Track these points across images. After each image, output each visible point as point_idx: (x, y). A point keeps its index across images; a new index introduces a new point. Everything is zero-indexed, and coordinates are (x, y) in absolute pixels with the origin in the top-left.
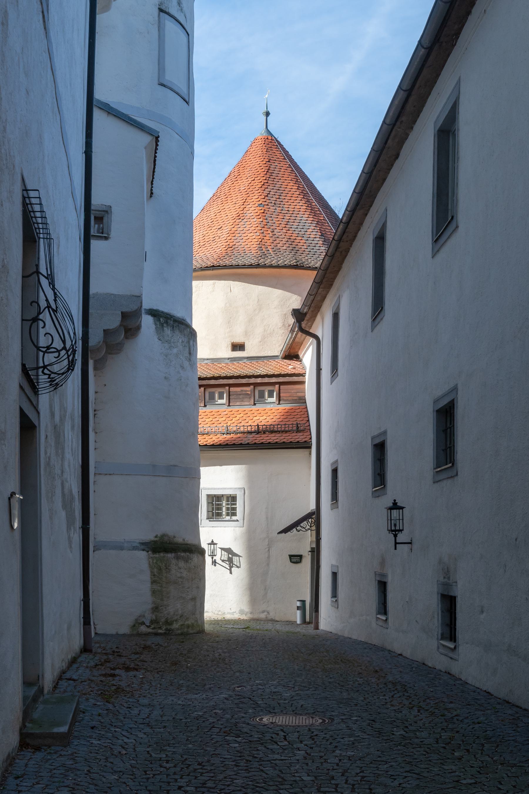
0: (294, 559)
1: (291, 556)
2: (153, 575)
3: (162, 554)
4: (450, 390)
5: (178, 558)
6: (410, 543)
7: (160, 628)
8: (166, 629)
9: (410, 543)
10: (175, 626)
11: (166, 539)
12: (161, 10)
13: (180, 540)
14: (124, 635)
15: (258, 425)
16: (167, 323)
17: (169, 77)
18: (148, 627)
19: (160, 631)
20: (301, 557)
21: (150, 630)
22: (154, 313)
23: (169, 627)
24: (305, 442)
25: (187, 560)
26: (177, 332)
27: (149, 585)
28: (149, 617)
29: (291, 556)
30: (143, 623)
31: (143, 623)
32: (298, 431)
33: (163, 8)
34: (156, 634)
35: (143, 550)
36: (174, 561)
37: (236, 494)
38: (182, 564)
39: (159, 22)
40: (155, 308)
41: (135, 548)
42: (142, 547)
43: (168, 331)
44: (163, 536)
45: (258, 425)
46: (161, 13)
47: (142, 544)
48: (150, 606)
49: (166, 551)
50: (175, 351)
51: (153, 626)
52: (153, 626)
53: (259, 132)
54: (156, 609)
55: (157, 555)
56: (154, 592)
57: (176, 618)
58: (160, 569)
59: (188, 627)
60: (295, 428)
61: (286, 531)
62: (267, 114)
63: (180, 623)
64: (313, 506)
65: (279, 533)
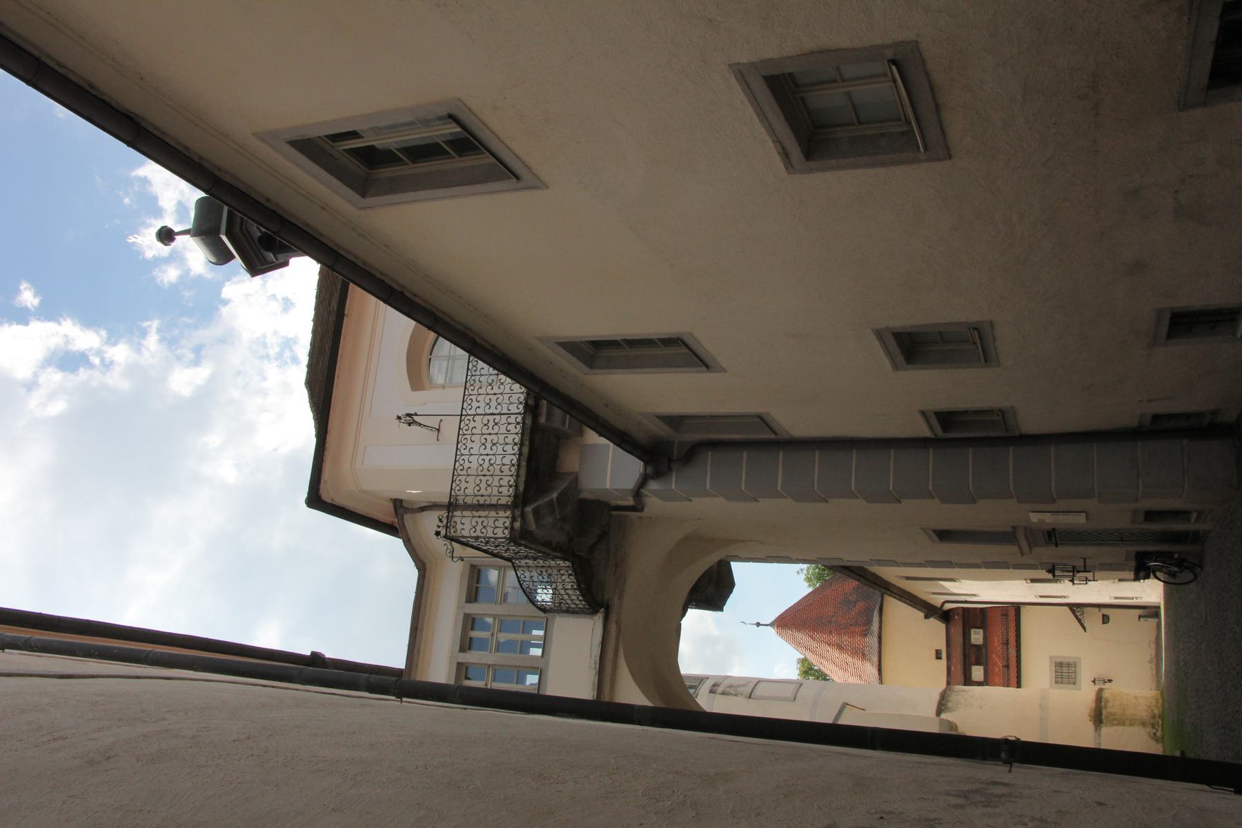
0: (1106, 621)
1: (1104, 623)
2: (1118, 725)
3: (1103, 717)
4: (748, 91)
5: (1106, 707)
6: (1085, 560)
7: (1158, 722)
8: (1159, 718)
9: (1085, 560)
10: (1156, 712)
11: (1092, 714)
12: (750, 697)
13: (1093, 705)
14: (1163, 747)
15: (1002, 644)
16: (944, 705)
17: (789, 694)
18: (1157, 730)
19: (1160, 722)
20: (1104, 616)
21: (1160, 729)
22: (939, 712)
23: (1157, 716)
24: (1015, 610)
25: (1107, 701)
26: (950, 698)
27: (1126, 728)
28: (1149, 729)
29: (1104, 623)
30: (1155, 734)
31: (1155, 734)
32: (1006, 615)
33: (748, 696)
34: (1162, 725)
35: (1100, 729)
36: (1108, 710)
37: (1080, 658)
38: (1110, 705)
39: (757, 699)
40: (935, 712)
41: (1099, 735)
42: (1098, 730)
43: (950, 705)
44: (1089, 715)
45: (1002, 644)
46: (752, 697)
47: (1096, 730)
48: (1141, 728)
49: (1101, 714)
50: (962, 701)
51: (1157, 727)
52: (1157, 727)
53: (772, 631)
54: (1143, 724)
55: (1104, 721)
56: (1131, 725)
57: (1150, 711)
58: (1114, 719)
59: (1157, 703)
60: (1004, 617)
61: (1084, 628)
62: (758, 624)
63: (1154, 708)
64: (1066, 608)
65: (1085, 631)
